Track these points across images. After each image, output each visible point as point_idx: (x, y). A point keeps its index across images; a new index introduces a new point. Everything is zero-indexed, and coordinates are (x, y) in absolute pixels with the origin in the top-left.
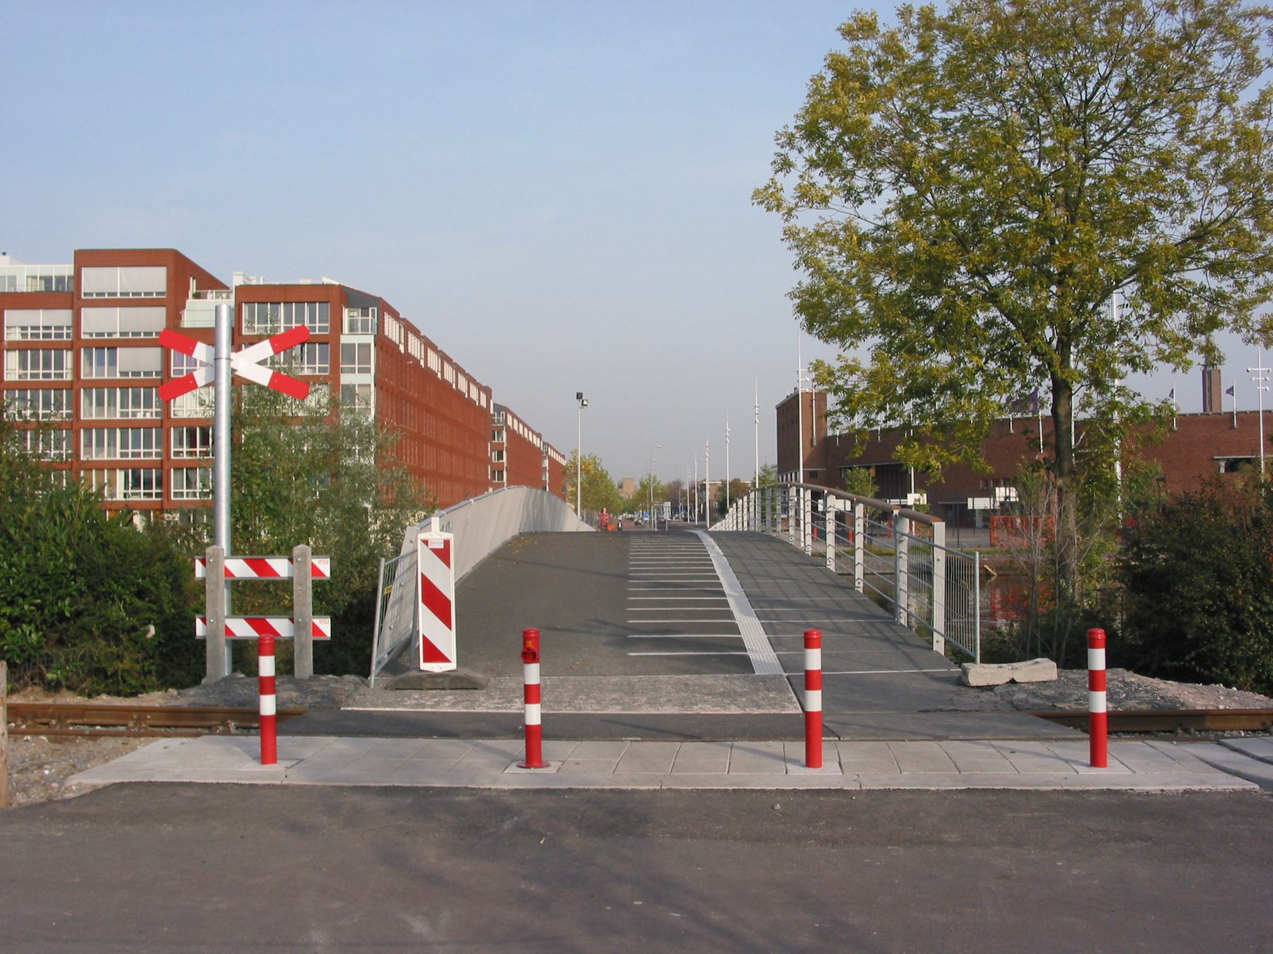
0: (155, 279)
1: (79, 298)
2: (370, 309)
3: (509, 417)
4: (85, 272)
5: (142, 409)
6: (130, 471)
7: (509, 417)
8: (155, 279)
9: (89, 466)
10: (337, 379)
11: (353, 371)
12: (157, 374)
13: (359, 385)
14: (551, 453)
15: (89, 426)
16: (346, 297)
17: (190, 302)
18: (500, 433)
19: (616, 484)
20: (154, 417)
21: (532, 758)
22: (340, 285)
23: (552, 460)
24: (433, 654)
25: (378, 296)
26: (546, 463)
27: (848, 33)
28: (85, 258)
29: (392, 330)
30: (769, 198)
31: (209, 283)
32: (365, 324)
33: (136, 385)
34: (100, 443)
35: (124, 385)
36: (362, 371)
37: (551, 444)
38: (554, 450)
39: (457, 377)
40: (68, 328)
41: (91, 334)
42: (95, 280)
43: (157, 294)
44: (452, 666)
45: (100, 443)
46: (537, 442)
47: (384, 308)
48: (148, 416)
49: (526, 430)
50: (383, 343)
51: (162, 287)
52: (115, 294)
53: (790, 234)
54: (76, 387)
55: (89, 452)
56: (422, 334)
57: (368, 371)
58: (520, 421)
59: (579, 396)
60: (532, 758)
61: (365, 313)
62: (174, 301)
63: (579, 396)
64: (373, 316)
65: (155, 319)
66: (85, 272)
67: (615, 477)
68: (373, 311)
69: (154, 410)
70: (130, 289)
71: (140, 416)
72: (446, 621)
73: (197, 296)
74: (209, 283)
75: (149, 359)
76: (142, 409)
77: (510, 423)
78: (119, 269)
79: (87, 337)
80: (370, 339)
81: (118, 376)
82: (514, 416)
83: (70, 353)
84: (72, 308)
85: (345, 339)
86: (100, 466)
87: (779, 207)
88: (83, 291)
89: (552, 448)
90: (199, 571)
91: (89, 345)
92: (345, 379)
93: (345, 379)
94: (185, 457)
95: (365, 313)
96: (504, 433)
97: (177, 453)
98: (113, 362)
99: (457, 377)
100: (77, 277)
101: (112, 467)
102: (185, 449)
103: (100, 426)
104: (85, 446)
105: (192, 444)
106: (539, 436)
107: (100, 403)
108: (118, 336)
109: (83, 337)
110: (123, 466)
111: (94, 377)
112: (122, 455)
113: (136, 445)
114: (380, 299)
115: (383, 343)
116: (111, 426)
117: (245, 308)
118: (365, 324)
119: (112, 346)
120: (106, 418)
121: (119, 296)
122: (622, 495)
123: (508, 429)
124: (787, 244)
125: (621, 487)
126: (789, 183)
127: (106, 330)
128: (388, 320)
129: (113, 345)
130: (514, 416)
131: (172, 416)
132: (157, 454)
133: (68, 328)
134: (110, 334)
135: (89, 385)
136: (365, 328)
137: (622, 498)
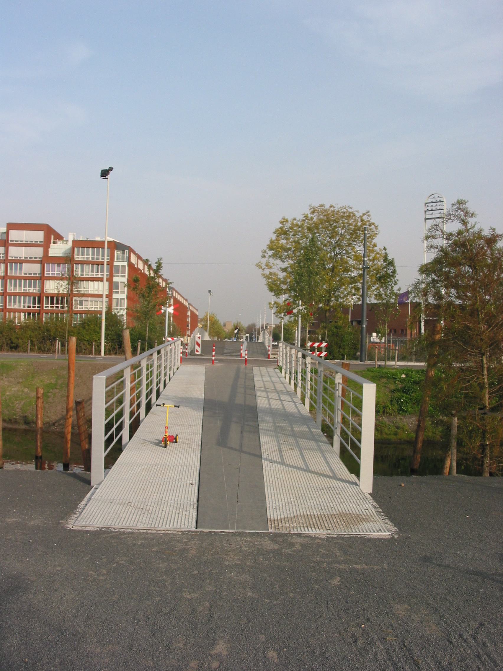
0: (39, 236)
1: (8, 242)
2: (125, 251)
3: (174, 292)
4: (11, 232)
5: (32, 289)
6: (27, 313)
7: (174, 292)
8: (39, 236)
9: (10, 311)
10: (112, 279)
11: (118, 276)
12: (39, 274)
13: (121, 282)
14: (192, 308)
15: (11, 294)
16: (115, 246)
17: (52, 245)
18: (170, 300)
19: (222, 324)
20: (37, 292)
21: (213, 363)
22: (113, 241)
23: (192, 313)
24: (197, 351)
25: (129, 246)
26: (189, 313)
27: (282, 222)
28: (11, 226)
29: (133, 259)
30: (259, 266)
31: (59, 237)
32: (123, 257)
33: (30, 278)
34: (15, 302)
35: (25, 279)
36: (122, 276)
37: (192, 304)
38: (193, 307)
39: (144, 267)
40: (3, 254)
41: (12, 257)
42: (15, 235)
43: (40, 242)
44: (200, 353)
45: (15, 302)
46: (186, 303)
47: (131, 250)
48: (35, 291)
49: (179, 296)
50: (131, 265)
51: (42, 239)
52: (23, 241)
53: (263, 275)
54: (6, 279)
55: (10, 305)
56: (136, 253)
57: (124, 276)
58: (179, 294)
59: (210, 291)
60: (213, 363)
61: (123, 253)
62: (46, 245)
63: (210, 291)
64: (126, 254)
65: (38, 252)
66: (11, 232)
67: (222, 322)
68: (127, 252)
69: (37, 289)
70: (29, 239)
71: (31, 291)
72: (199, 347)
73: (54, 243)
74: (59, 237)
75: (35, 269)
76: (32, 289)
77: (174, 295)
78: (24, 231)
79: (11, 258)
80: (126, 264)
81: (23, 275)
82: (176, 292)
83: (3, 264)
84: (5, 246)
85: (115, 263)
86: (15, 311)
87: (261, 268)
88: (10, 239)
89: (192, 306)
90: (164, 339)
91: (12, 262)
92: (115, 279)
93: (115, 279)
94: (50, 308)
95: (123, 253)
96: (172, 300)
97: (46, 307)
98: (21, 269)
99: (144, 267)
100: (7, 233)
101: (20, 311)
102: (49, 305)
103: (15, 294)
104: (9, 302)
105: (52, 303)
106: (186, 300)
107: (15, 285)
108: (23, 258)
109: (9, 258)
110: (24, 311)
111: (13, 275)
112: (24, 307)
113: (29, 303)
114: (129, 247)
115: (131, 265)
116: (20, 295)
117: (76, 249)
118: (123, 257)
119: (21, 262)
120: (17, 291)
121: (24, 242)
122: (225, 330)
123: (174, 297)
124: (262, 277)
125: (225, 326)
126: (264, 261)
127: (19, 256)
128: (133, 256)
129: (21, 262)
130: (176, 292)
131: (45, 292)
132: (38, 307)
133: (3, 254)
134: (20, 258)
135: (11, 278)
136: (123, 259)
137: (225, 331)
